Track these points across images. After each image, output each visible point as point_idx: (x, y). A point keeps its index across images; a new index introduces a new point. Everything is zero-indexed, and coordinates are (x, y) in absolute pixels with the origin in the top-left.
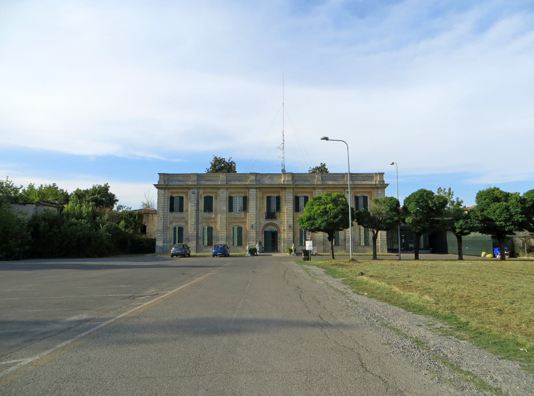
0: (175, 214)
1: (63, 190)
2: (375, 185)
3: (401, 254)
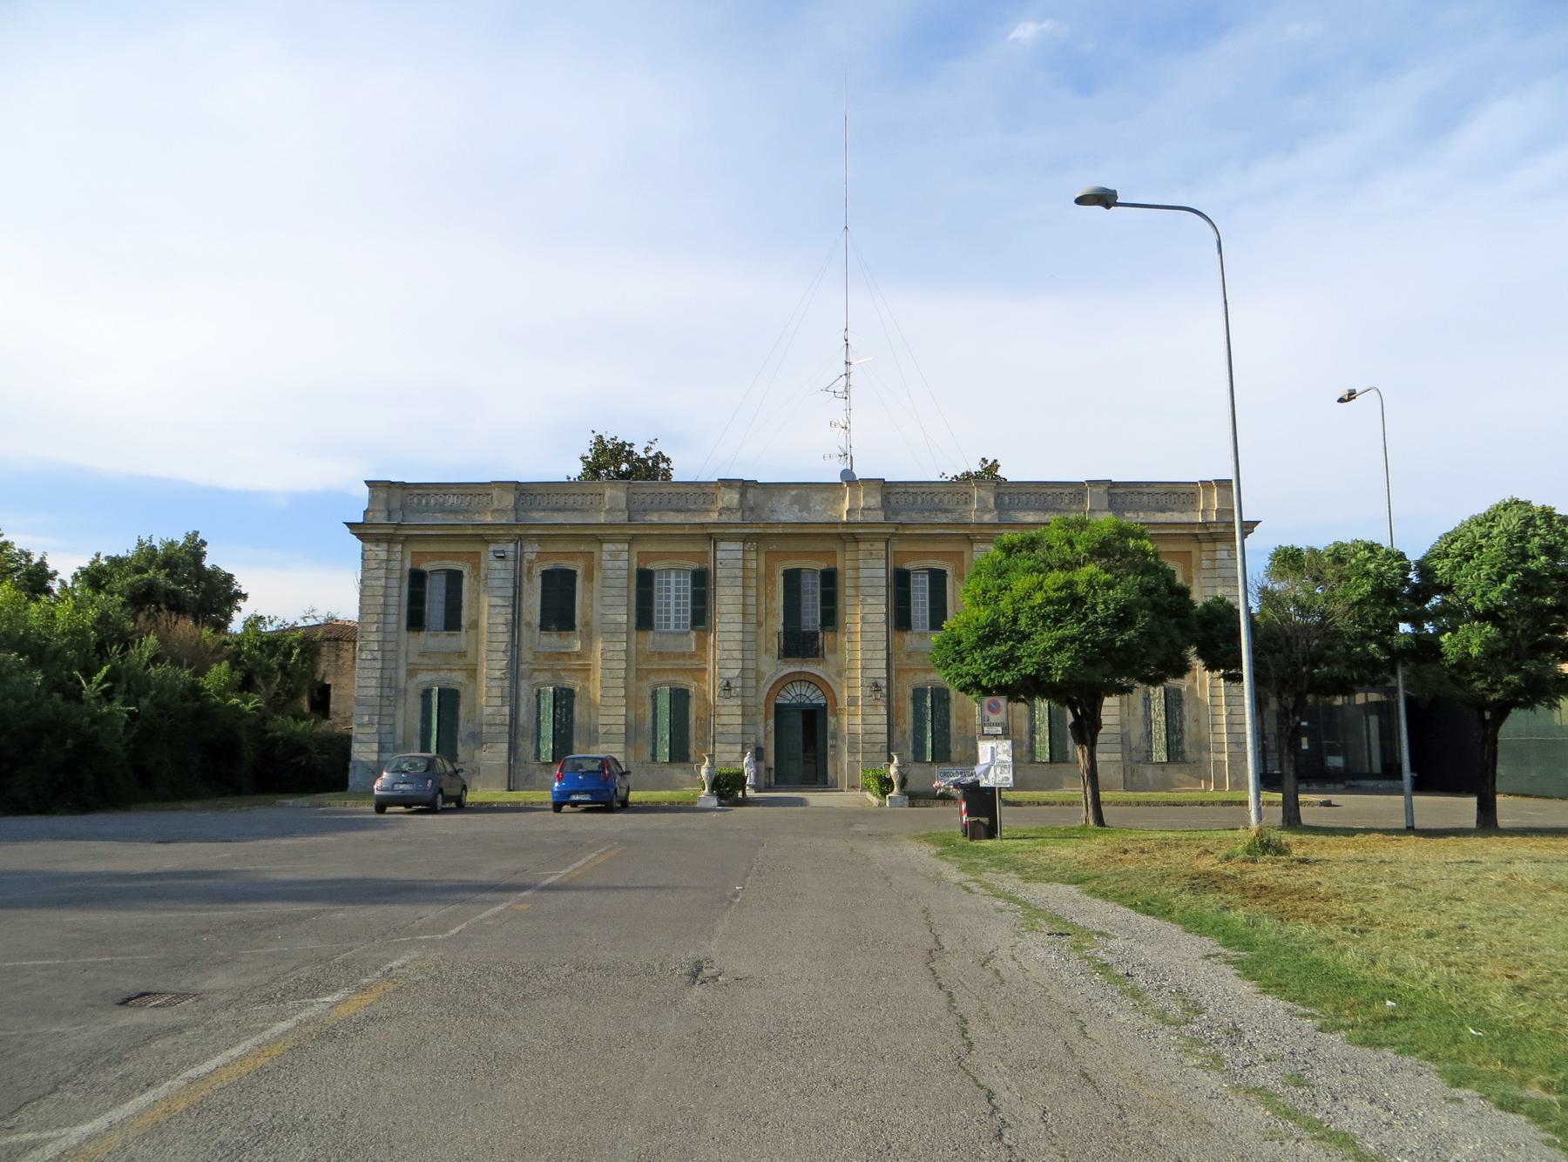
0: (435, 639)
1: (27, 555)
2: (1204, 525)
3: (1420, 800)
